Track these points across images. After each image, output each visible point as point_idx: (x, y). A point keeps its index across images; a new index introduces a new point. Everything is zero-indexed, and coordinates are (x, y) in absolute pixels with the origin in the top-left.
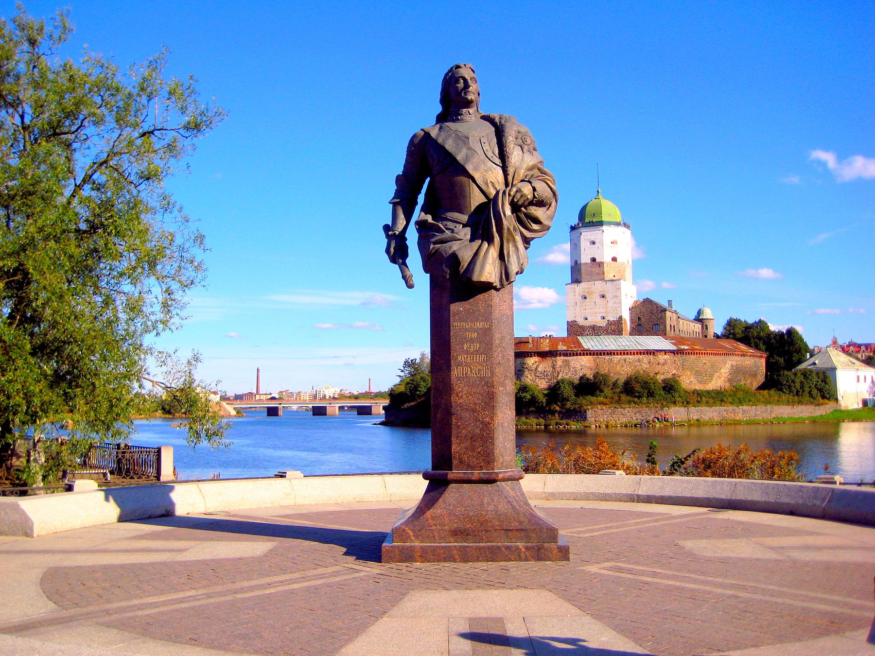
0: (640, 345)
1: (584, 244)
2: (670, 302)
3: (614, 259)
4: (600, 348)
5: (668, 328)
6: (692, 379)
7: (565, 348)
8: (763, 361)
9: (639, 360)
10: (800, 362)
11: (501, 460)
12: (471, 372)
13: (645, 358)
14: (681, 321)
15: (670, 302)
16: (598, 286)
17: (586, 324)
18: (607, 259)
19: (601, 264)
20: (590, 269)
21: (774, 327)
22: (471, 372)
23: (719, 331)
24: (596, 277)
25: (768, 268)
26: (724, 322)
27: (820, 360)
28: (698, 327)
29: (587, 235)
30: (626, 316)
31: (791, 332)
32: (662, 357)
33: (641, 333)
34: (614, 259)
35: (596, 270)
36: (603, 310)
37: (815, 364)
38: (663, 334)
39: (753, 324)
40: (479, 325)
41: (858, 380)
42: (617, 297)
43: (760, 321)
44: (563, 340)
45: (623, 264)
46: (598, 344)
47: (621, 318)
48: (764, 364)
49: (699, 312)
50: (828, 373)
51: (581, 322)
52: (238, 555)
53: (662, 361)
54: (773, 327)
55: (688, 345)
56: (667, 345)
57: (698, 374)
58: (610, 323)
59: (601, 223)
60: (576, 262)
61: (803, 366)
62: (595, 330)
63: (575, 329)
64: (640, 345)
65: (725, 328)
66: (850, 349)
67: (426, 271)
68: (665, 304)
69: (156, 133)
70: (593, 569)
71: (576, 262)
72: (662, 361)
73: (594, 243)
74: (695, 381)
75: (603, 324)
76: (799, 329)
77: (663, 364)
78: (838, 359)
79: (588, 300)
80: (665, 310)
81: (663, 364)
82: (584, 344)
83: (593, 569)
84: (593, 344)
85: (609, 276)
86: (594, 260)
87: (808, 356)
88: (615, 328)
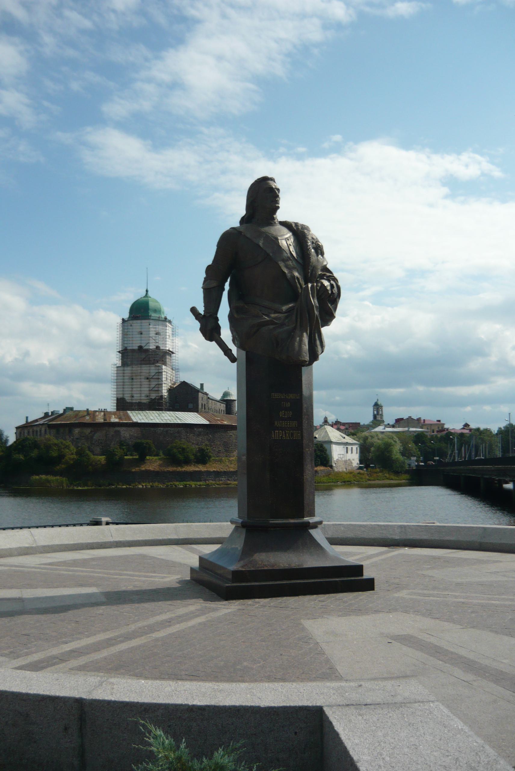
0: (180, 419)
2: (202, 385)
5: (200, 407)
7: (117, 420)
9: (178, 432)
12: (286, 436)
14: (210, 401)
15: (202, 385)
22: (286, 436)
27: (320, 435)
29: (137, 324)
30: (165, 393)
38: (195, 409)
40: (291, 396)
41: (347, 452)
46: (144, 418)
50: (325, 446)
51: (128, 398)
62: (141, 407)
64: (180, 419)
68: (199, 387)
78: (334, 434)
82: (133, 418)
84: (141, 418)
88: (155, 405)
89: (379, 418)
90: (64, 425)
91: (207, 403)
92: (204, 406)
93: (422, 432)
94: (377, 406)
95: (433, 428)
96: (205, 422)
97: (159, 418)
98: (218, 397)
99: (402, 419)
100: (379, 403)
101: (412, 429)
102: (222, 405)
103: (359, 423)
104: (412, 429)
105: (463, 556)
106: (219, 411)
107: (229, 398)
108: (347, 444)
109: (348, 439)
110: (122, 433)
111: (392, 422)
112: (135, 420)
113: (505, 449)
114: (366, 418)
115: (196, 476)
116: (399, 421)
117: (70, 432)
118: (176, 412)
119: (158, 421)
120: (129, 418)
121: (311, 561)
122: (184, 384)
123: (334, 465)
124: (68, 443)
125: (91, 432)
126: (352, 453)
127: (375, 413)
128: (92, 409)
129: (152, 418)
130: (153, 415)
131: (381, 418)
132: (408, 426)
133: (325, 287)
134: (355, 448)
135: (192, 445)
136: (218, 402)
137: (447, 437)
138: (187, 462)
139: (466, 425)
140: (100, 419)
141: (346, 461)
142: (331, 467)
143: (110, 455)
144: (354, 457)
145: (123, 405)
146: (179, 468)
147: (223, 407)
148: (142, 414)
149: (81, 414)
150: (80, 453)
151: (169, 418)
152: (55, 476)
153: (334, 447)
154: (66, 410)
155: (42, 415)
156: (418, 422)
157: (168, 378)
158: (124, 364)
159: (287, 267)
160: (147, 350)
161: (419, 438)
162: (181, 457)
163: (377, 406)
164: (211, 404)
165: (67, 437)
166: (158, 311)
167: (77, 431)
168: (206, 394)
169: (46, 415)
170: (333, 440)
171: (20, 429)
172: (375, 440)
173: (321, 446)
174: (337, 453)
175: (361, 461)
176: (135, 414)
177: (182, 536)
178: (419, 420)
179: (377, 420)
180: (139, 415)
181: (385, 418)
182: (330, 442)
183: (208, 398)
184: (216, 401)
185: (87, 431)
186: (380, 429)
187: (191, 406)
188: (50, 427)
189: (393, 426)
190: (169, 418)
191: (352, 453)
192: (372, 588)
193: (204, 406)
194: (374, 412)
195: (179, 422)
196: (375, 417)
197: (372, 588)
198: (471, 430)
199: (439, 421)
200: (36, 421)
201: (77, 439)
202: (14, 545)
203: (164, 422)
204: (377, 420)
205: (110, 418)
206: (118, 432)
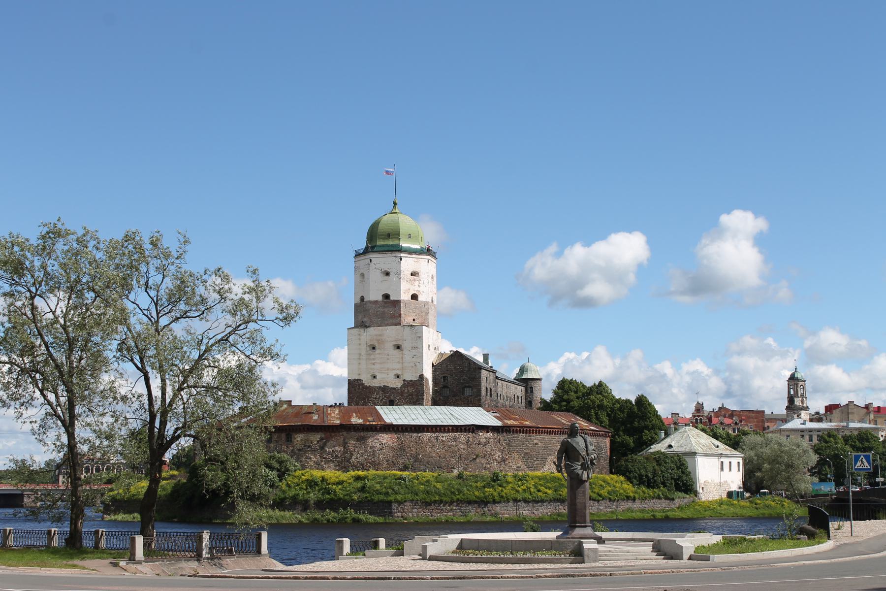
0: (457, 419)
1: (375, 276)
3: (414, 297)
4: (406, 422)
5: (483, 393)
6: (520, 464)
7: (360, 421)
8: (608, 440)
9: (455, 439)
10: (653, 441)
13: (462, 437)
14: (499, 383)
15: (486, 357)
16: (390, 333)
17: (376, 383)
18: (405, 297)
19: (397, 303)
20: (381, 309)
21: (624, 391)
23: (548, 396)
24: (391, 321)
27: (678, 442)
28: (520, 390)
29: (380, 261)
30: (428, 374)
31: (642, 402)
32: (483, 436)
33: (445, 403)
34: (414, 297)
35: (390, 311)
36: (399, 366)
37: (670, 446)
39: (591, 388)
41: (722, 469)
42: (417, 348)
43: (642, 402)
45: (426, 303)
46: (402, 417)
47: (421, 376)
48: (608, 445)
49: (523, 370)
50: (688, 460)
51: (367, 381)
53: (483, 440)
55: (515, 419)
56: (489, 419)
57: (527, 457)
58: (407, 384)
59: (398, 249)
60: (362, 299)
61: (655, 448)
62: (392, 397)
63: (359, 392)
64: (457, 419)
65: (555, 392)
66: (702, 420)
68: (480, 359)
71: (362, 299)
72: (483, 440)
73: (388, 274)
74: (523, 467)
75: (398, 384)
77: (485, 444)
78: (695, 439)
79: (377, 351)
80: (480, 368)
81: (485, 444)
82: (384, 417)
84: (397, 417)
85: (407, 319)
86: (387, 296)
87: (663, 436)
88: (411, 393)
89: (798, 402)
91: (495, 386)
92: (489, 391)
93: (867, 429)
97: (424, 416)
98: (513, 374)
99: (837, 406)
100: (798, 375)
102: (519, 388)
103: (763, 412)
104: (852, 425)
108: (721, 455)
112: (388, 421)
117: (289, 439)
118: (451, 408)
120: (380, 417)
123: (700, 490)
125: (321, 439)
126: (730, 470)
127: (792, 392)
129: (414, 417)
130: (415, 412)
131: (802, 402)
134: (734, 461)
136: (513, 383)
142: (696, 493)
144: (734, 479)
146: (175, 452)
148: (398, 411)
151: (440, 416)
152: (130, 512)
153: (483, 372)
164: (502, 389)
165: (284, 447)
167: (299, 438)
170: (699, 450)
175: (746, 486)
176: (387, 411)
180: (393, 412)
182: (693, 454)
183: (497, 378)
184: (509, 382)
185: (316, 438)
190: (440, 416)
191: (730, 470)
193: (489, 391)
194: (789, 392)
196: (791, 400)
201: (300, 450)
203: (433, 423)
205: (350, 417)
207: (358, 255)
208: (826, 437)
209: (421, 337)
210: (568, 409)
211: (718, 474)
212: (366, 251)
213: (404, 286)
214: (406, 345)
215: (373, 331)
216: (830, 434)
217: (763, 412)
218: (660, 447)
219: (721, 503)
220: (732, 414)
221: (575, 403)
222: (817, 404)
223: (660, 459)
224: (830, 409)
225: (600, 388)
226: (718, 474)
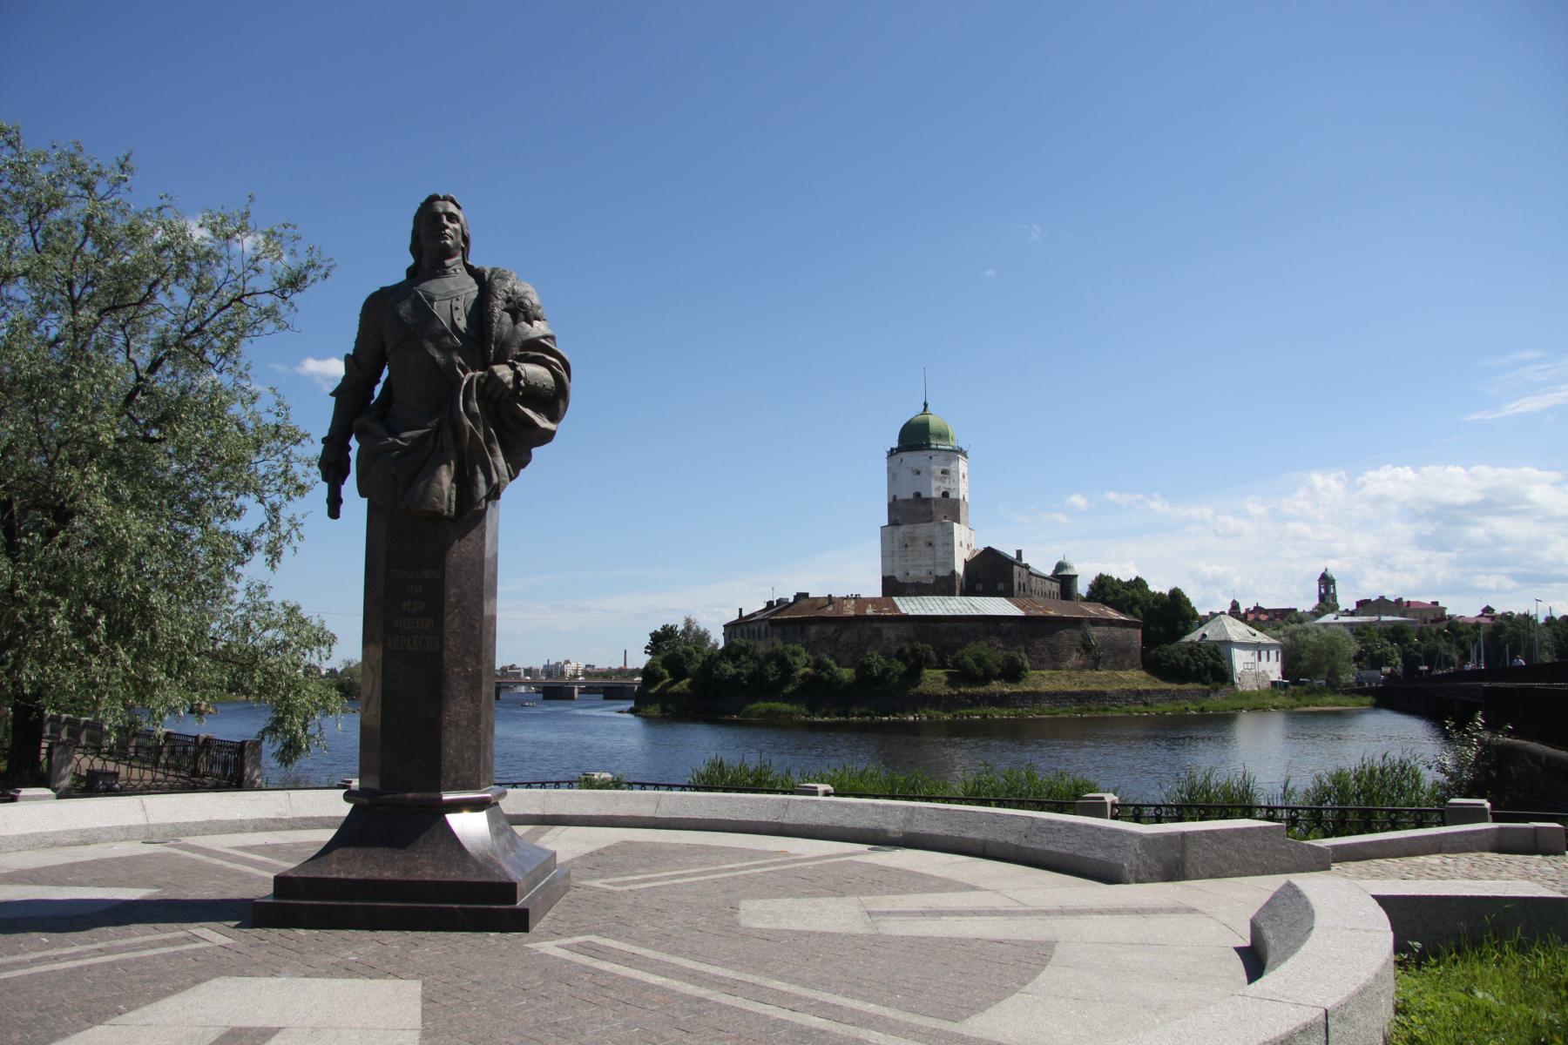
2: (1019, 553)
3: (945, 494)
8: (1139, 633)
10: (1187, 632)
11: (453, 776)
15: (1019, 553)
16: (922, 530)
21: (1159, 585)
25: (344, 379)
26: (1092, 578)
29: (912, 459)
30: (960, 569)
31: (1176, 595)
34: (945, 494)
38: (1008, 593)
42: (949, 544)
44: (873, 601)
47: (953, 572)
50: (1222, 650)
51: (899, 575)
52: (70, 860)
54: (1154, 587)
59: (927, 447)
60: (895, 498)
61: (1187, 638)
62: (919, 589)
67: (362, 494)
69: (245, 299)
70: (597, 883)
76: (339, 641)
78: (1237, 631)
83: (597, 883)
86: (918, 495)
88: (944, 586)
90: (793, 621)
92: (1023, 587)
94: (1326, 581)
95: (1425, 615)
96: (1018, 612)
100: (1329, 573)
101: (1384, 618)
104: (1384, 618)
105: (132, 891)
106: (1049, 595)
107: (1065, 573)
109: (1261, 637)
110: (885, 631)
111: (1353, 607)
113: (1561, 651)
114: (1306, 602)
115: (1003, 701)
116: (1363, 605)
119: (940, 612)
120: (895, 607)
121: (425, 868)
122: (989, 551)
124: (798, 648)
128: (836, 594)
132: (1379, 614)
133: (499, 381)
135: (994, 652)
137: (1455, 629)
138: (985, 679)
139: (1488, 610)
140: (849, 610)
141: (1257, 675)
143: (863, 669)
144: (1272, 669)
145: (892, 586)
147: (1055, 587)
149: (820, 604)
150: (819, 665)
153: (1236, 652)
154: (801, 596)
155: (764, 606)
156: (1399, 606)
157: (966, 543)
158: (893, 522)
159: (439, 348)
160: (928, 500)
161: (1396, 634)
162: (980, 672)
163: (1326, 581)
166: (943, 435)
168: (1027, 567)
169: (770, 604)
170: (1235, 638)
171: (730, 628)
172: (1310, 637)
173: (1216, 649)
174: (1241, 661)
175: (1285, 674)
177: (536, 811)
178: (1399, 601)
179: (1327, 599)
181: (1340, 600)
182: (1229, 643)
185: (830, 630)
186: (1329, 618)
187: (1001, 586)
188: (773, 623)
189: (1352, 614)
192: (525, 928)
193: (1023, 587)
195: (975, 613)
196: (1322, 598)
197: (525, 928)
198: (1493, 618)
199: (1436, 603)
200: (753, 615)
202: (200, 817)
204: (1327, 599)
206: (878, 632)
207: (892, 453)
208: (1358, 631)
209: (952, 534)
210: (1105, 602)
211: (1256, 666)
212: (899, 450)
213: (935, 484)
214: (938, 542)
215: (903, 528)
216: (1365, 626)
217: (554, 854)
218: (1195, 636)
219: (1259, 694)
220: (1266, 612)
221: (1110, 598)
222: (1346, 600)
223: (1193, 649)
224: (1360, 604)
225: (1139, 583)
226: (1256, 666)
